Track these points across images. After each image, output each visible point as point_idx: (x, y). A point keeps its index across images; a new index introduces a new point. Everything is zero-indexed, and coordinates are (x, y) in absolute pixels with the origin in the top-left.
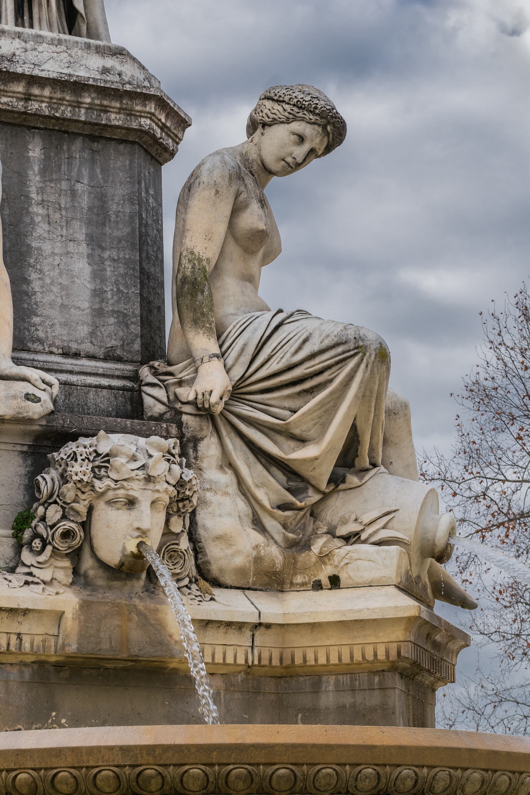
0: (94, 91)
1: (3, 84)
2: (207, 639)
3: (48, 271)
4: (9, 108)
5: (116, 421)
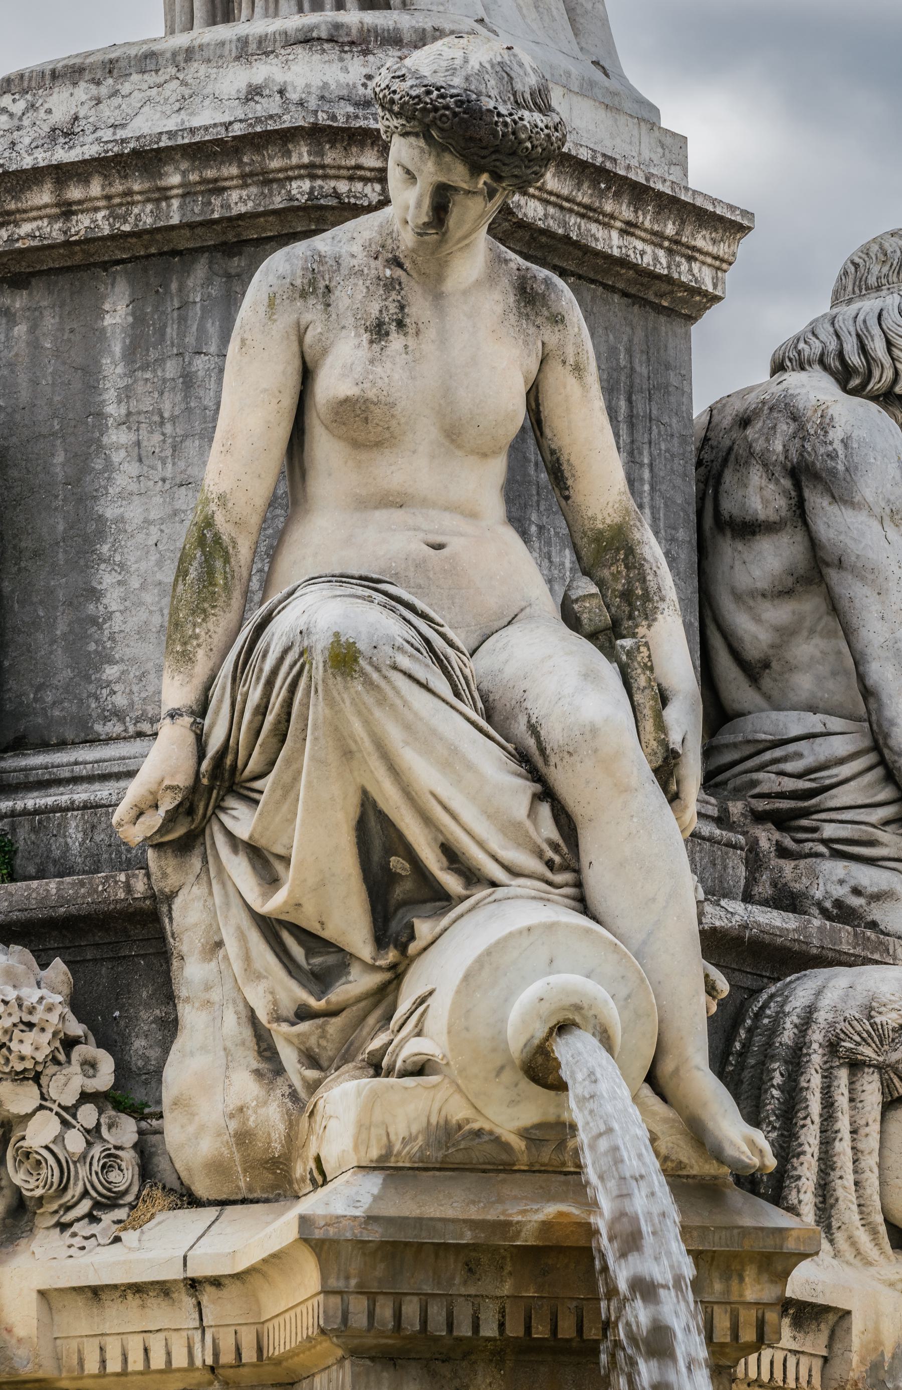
0: (182, 155)
1: (13, 197)
2: (107, 1325)
3: (136, 562)
4: (36, 243)
5: (28, 888)
